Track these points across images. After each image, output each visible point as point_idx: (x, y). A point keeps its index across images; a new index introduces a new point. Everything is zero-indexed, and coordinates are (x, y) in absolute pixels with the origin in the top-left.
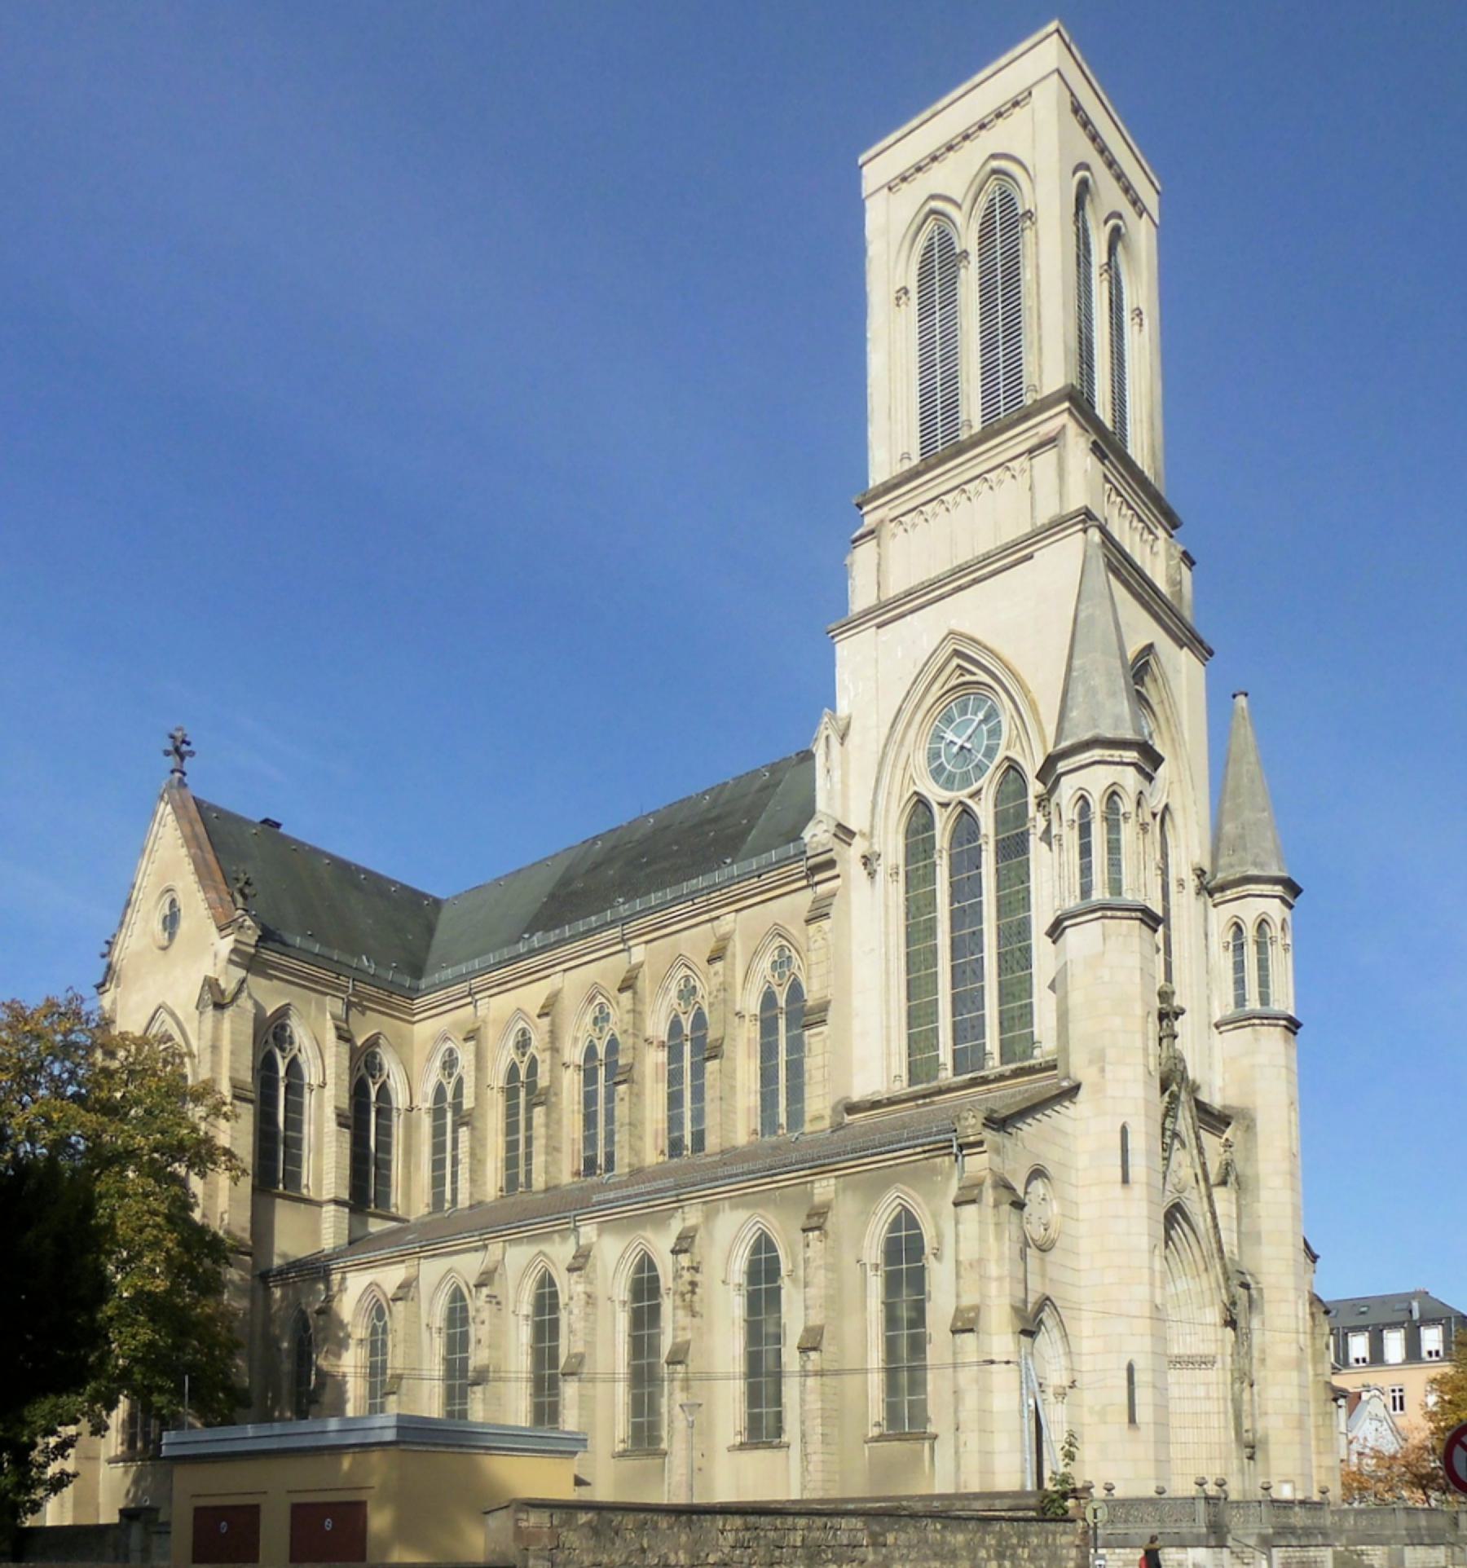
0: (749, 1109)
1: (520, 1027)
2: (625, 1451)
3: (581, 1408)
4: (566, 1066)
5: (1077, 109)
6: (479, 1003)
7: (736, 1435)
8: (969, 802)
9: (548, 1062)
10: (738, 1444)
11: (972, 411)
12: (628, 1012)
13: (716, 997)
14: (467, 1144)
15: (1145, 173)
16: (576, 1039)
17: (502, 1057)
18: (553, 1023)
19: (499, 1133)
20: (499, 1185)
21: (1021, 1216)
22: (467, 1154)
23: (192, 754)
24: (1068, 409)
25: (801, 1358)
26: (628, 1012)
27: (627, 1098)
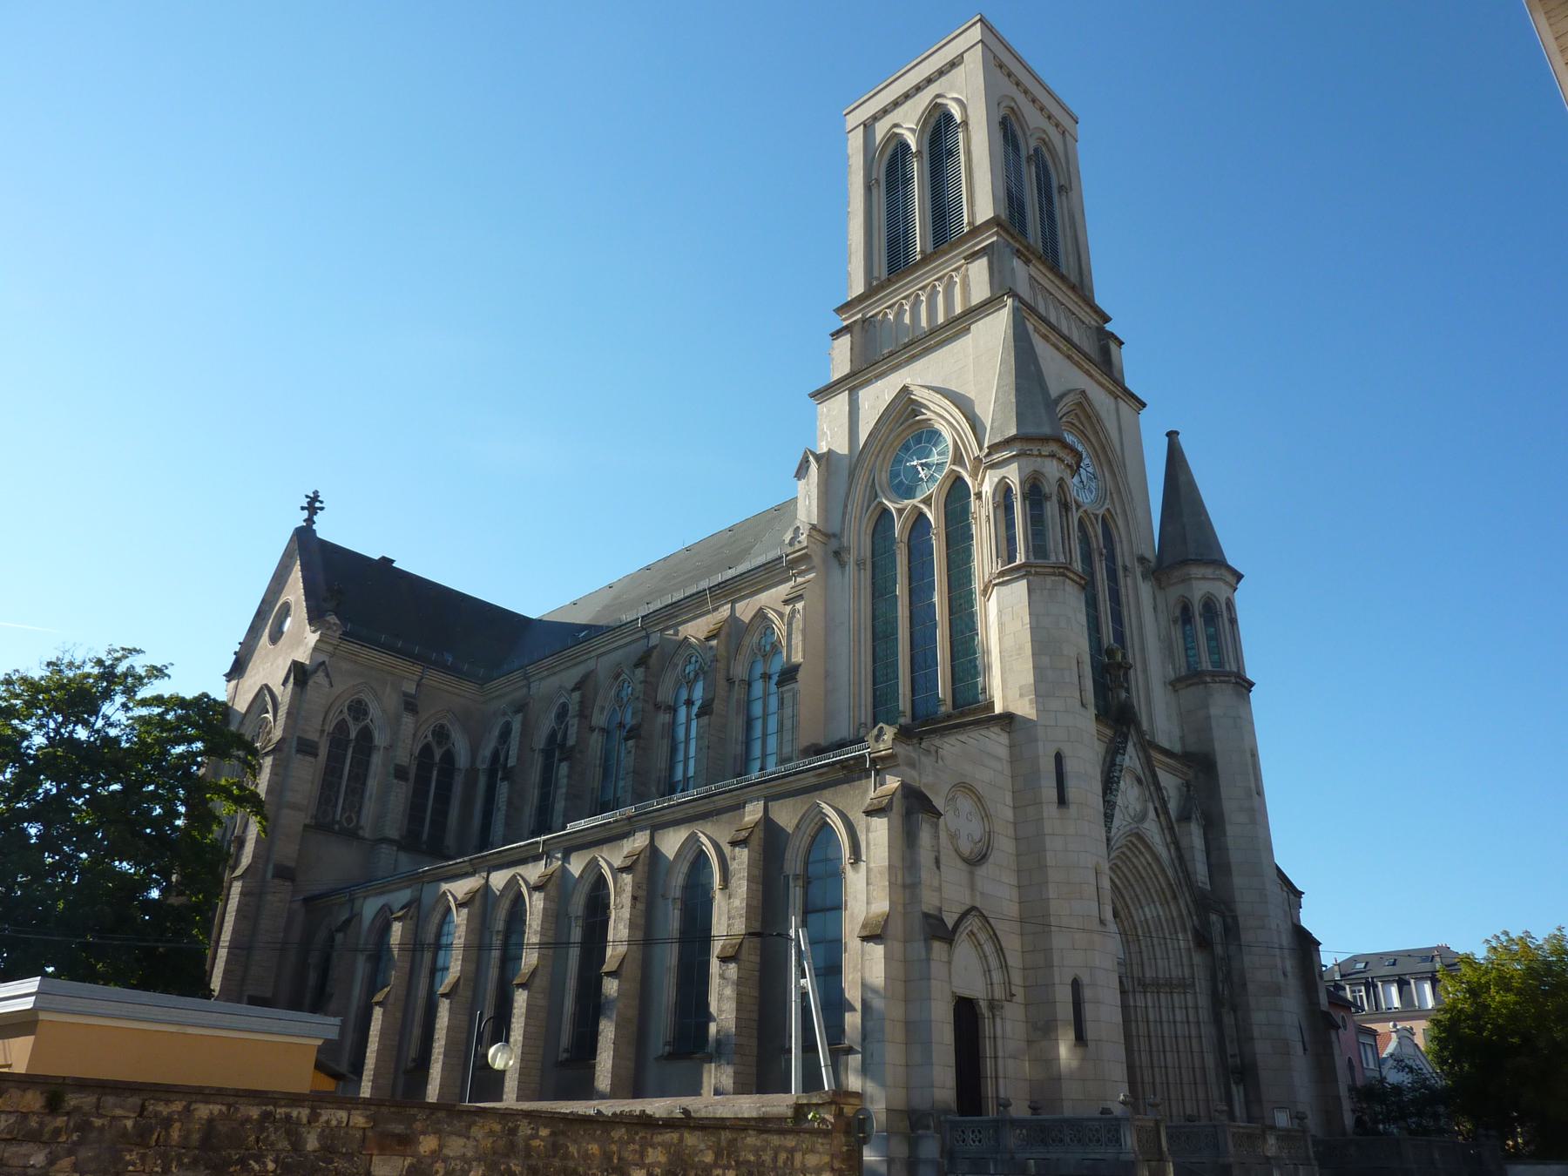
0: (663, 724)
1: (561, 701)
2: (567, 1060)
3: (908, 1043)
4: (592, 729)
5: (1001, 66)
6: (532, 685)
7: (665, 1045)
8: (922, 506)
9: (576, 727)
10: (665, 1054)
11: (919, 240)
12: (641, 683)
13: (709, 667)
14: (506, 795)
15: (1058, 102)
16: (603, 708)
17: (546, 724)
18: (583, 696)
19: (536, 786)
20: (532, 828)
21: (937, 825)
22: (505, 803)
23: (322, 509)
24: (997, 231)
25: (720, 967)
26: (641, 683)
27: (633, 751)
